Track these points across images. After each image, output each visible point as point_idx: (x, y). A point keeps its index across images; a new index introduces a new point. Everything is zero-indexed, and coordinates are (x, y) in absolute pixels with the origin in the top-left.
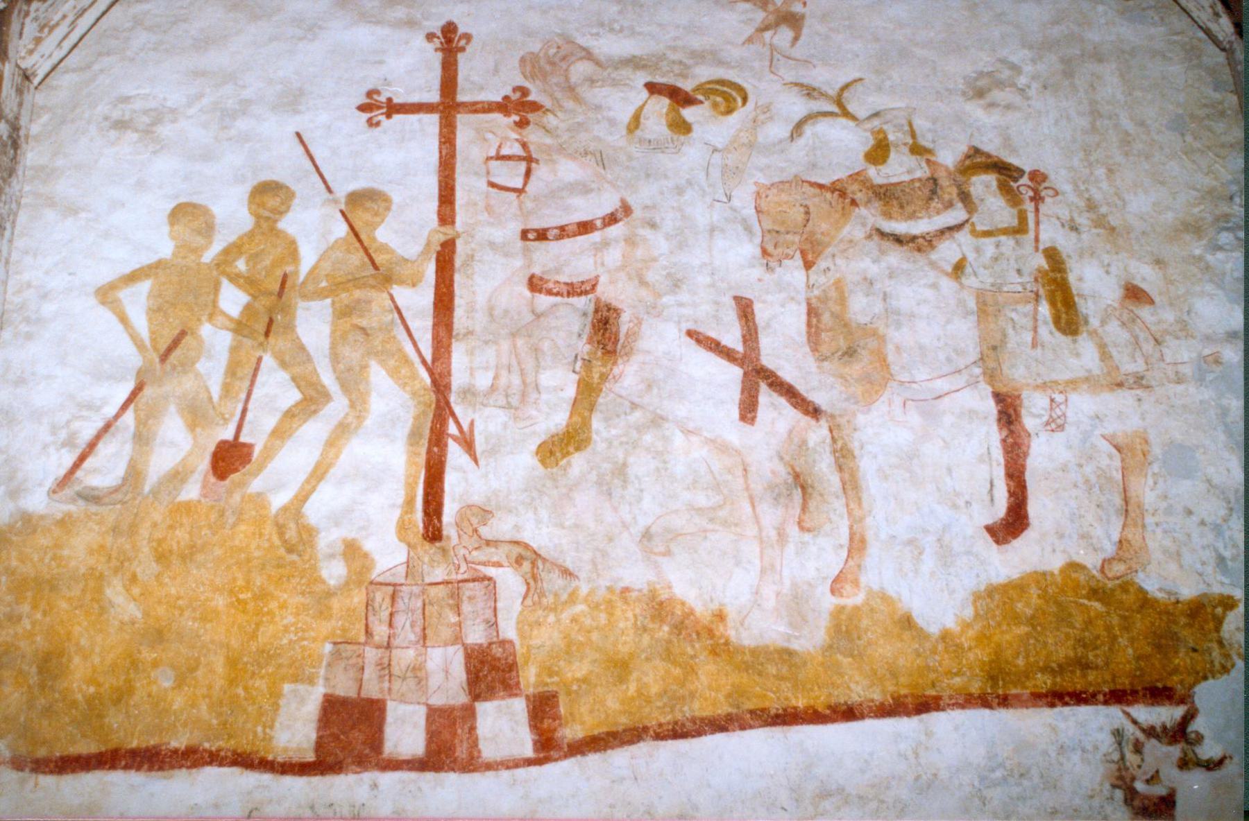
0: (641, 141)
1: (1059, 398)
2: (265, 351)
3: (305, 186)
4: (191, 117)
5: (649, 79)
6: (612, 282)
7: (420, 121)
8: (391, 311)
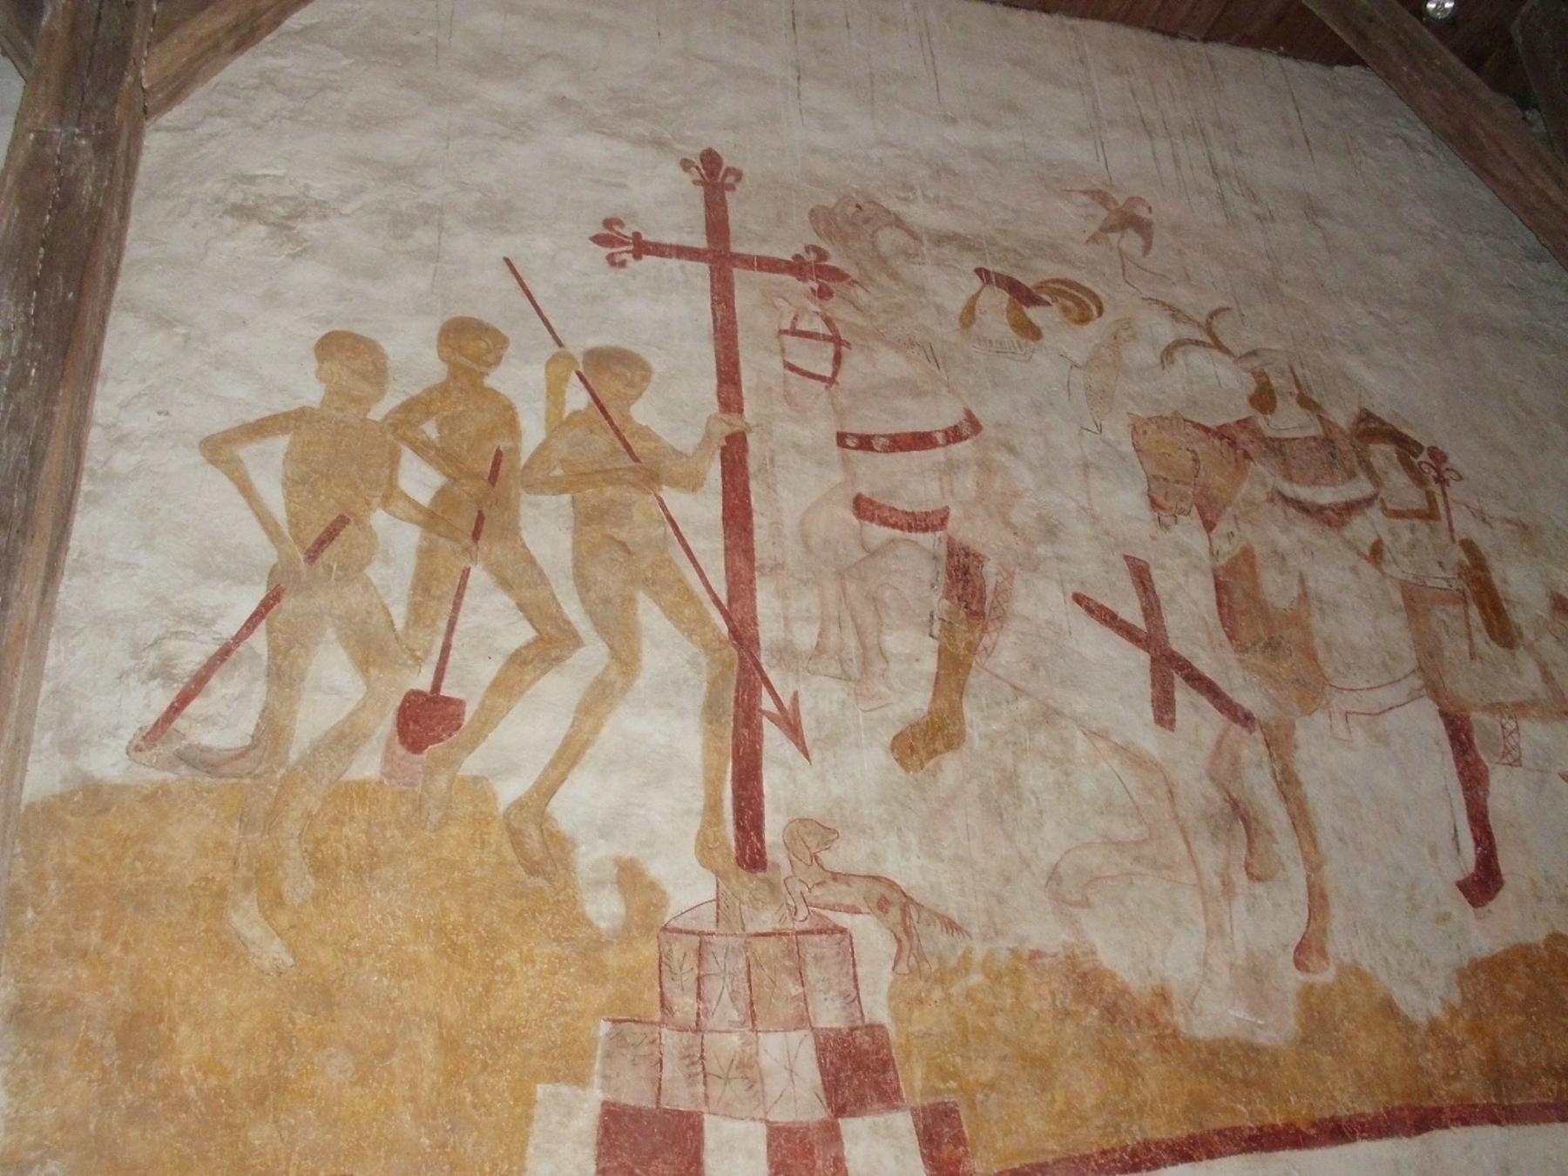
0: (980, 340)
1: (1511, 725)
2: (474, 560)
3: (523, 333)
4: (347, 216)
5: (981, 264)
6: (968, 517)
7: (682, 268)
8: (661, 522)
